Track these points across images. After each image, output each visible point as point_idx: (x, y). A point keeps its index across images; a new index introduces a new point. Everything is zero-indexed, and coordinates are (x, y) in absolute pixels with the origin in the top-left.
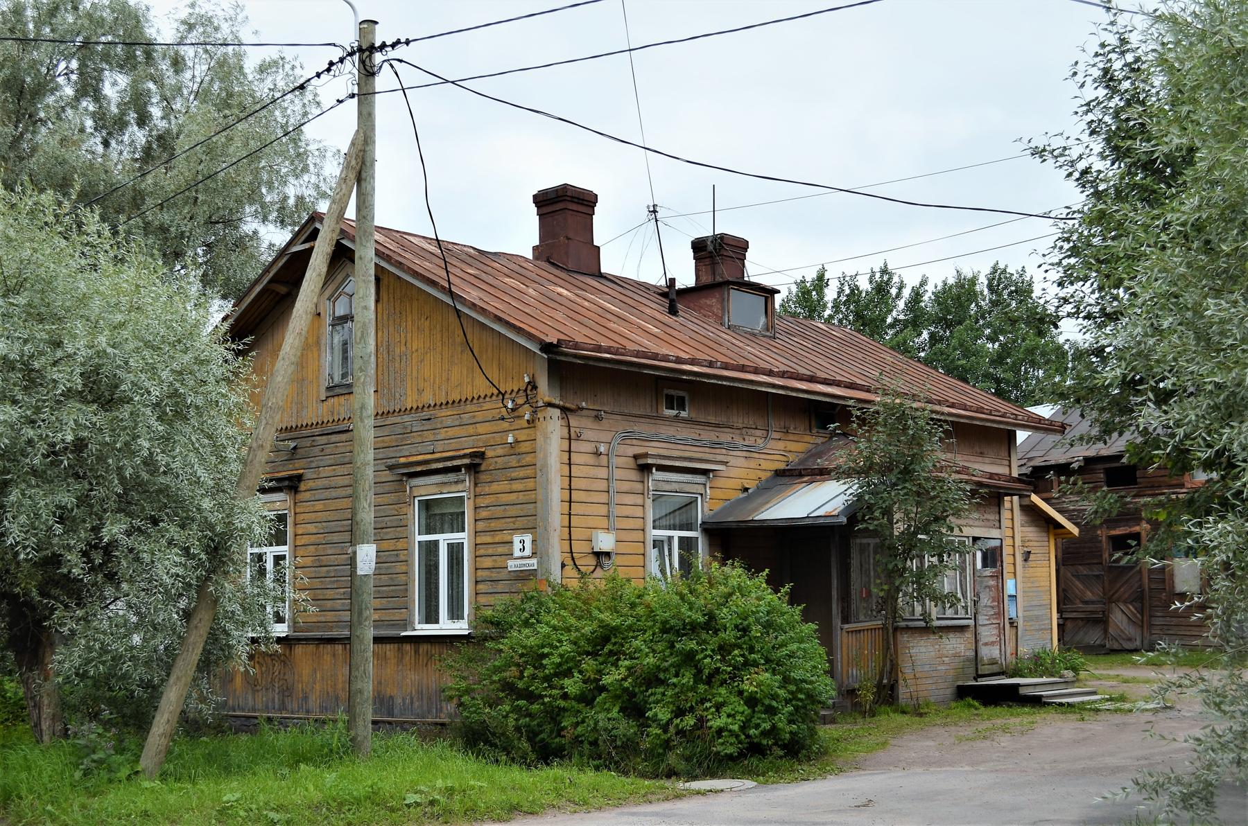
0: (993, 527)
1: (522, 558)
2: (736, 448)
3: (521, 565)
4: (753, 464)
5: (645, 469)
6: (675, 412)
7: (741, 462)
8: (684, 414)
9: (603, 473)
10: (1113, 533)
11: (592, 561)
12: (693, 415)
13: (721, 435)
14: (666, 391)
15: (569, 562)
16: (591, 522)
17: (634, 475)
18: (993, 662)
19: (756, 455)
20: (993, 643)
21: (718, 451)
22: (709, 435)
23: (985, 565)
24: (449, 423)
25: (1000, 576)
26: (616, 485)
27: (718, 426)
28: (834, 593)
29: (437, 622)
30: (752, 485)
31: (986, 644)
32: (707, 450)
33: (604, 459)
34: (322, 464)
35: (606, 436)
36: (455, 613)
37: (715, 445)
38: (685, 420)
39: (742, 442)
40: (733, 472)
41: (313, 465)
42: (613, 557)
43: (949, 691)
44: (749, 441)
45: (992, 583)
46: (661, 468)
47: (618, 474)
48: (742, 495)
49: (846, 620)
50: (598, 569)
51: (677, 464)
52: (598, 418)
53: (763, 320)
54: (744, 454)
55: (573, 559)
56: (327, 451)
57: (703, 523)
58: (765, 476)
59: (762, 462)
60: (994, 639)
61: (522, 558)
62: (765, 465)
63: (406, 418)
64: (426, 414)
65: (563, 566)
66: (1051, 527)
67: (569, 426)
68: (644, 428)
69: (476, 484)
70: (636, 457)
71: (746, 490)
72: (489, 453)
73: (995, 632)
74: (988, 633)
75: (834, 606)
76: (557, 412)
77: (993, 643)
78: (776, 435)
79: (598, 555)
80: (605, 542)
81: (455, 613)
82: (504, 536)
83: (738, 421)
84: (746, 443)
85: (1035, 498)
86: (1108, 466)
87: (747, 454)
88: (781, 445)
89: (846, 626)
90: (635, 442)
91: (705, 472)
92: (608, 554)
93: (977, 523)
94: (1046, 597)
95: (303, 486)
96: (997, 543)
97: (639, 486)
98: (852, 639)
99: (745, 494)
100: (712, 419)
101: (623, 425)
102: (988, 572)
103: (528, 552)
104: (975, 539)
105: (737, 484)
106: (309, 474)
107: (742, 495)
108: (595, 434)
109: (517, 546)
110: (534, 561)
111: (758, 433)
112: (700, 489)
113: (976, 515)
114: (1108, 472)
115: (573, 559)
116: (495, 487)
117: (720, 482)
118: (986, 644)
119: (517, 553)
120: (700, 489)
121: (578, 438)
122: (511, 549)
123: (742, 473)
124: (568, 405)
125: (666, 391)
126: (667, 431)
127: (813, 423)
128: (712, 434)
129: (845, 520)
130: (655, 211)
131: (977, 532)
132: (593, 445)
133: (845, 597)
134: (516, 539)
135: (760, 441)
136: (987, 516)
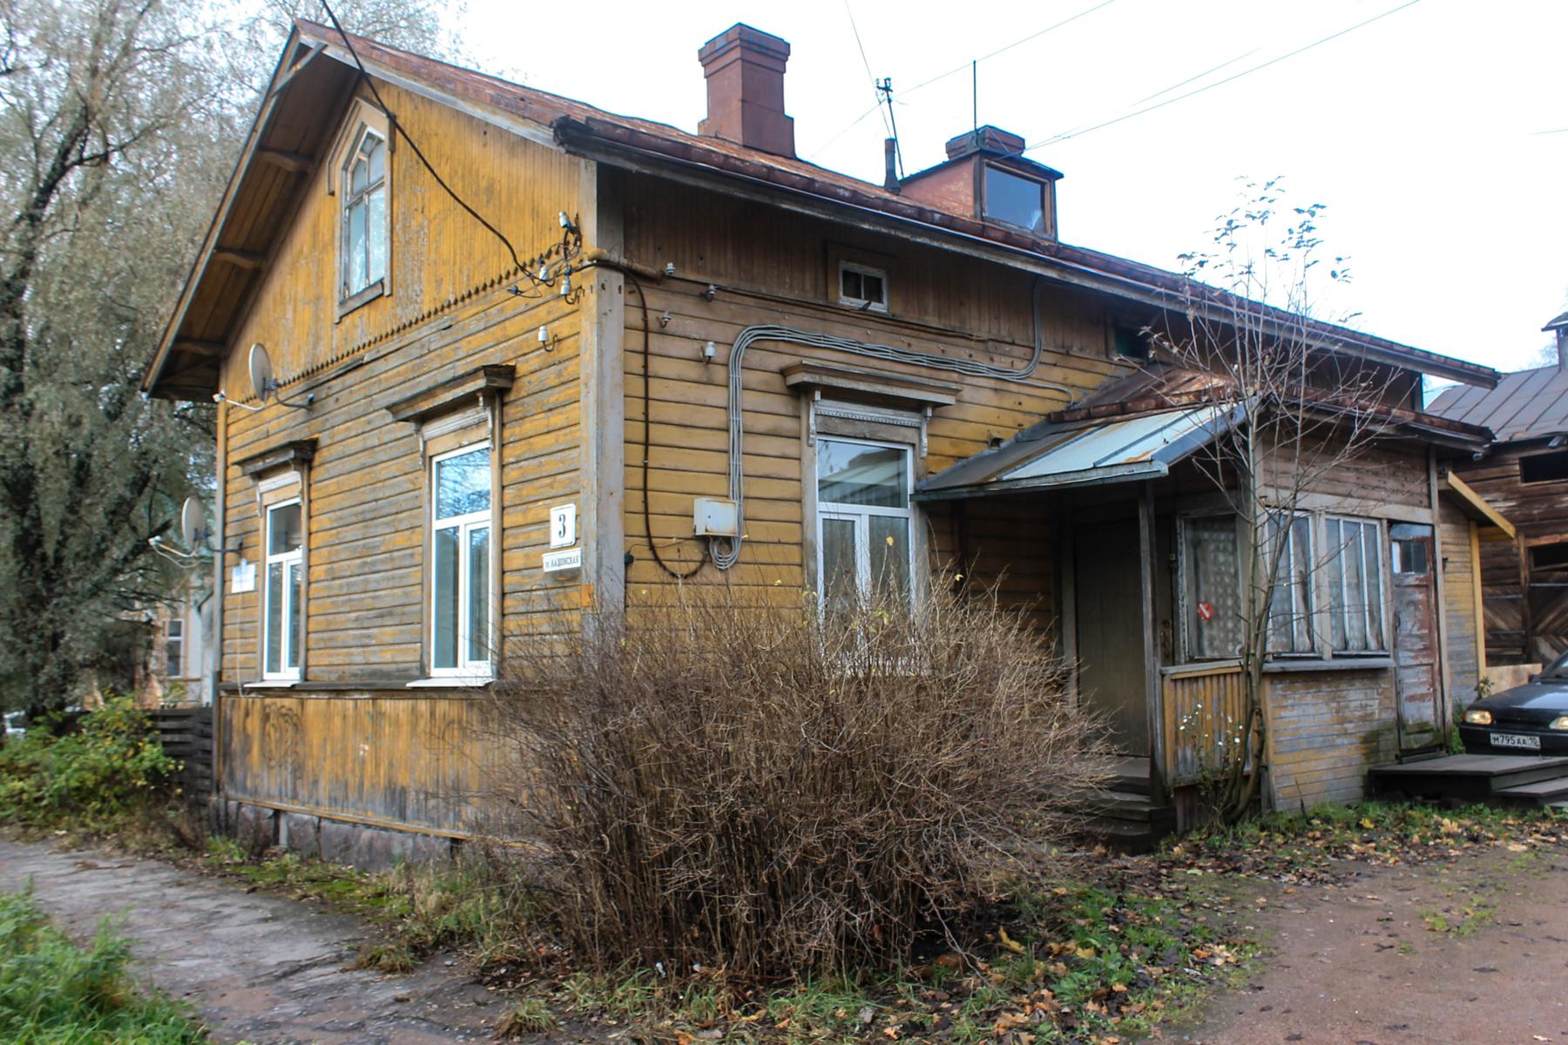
0: (1420, 504)
1: (562, 548)
2: (976, 373)
3: (561, 562)
4: (1008, 402)
5: (800, 393)
6: (861, 303)
7: (988, 397)
8: (875, 307)
9: (717, 396)
10: (1545, 541)
11: (694, 552)
12: (898, 310)
13: (949, 349)
14: (844, 265)
15: (642, 551)
16: (690, 482)
17: (779, 404)
18: (1423, 728)
19: (1013, 388)
20: (1422, 697)
21: (944, 375)
22: (928, 348)
23: (1406, 565)
24: (473, 328)
25: (1430, 585)
26: (740, 420)
27: (942, 333)
28: (1147, 609)
29: (455, 665)
30: (1008, 436)
31: (1412, 698)
32: (924, 372)
33: (719, 374)
34: (336, 421)
35: (726, 333)
36: (478, 653)
37: (937, 364)
38: (878, 316)
39: (987, 363)
40: (971, 413)
41: (328, 425)
42: (737, 547)
43: (1357, 782)
44: (1002, 363)
45: (1419, 596)
46: (831, 393)
47: (750, 400)
48: (987, 451)
49: (1170, 657)
50: (707, 570)
51: (862, 386)
52: (705, 298)
53: (1038, 214)
54: (992, 383)
55: (652, 548)
56: (342, 402)
57: (917, 492)
58: (1028, 422)
59: (1024, 400)
60: (1424, 690)
61: (562, 548)
62: (1029, 404)
63: (425, 331)
64: (445, 320)
65: (629, 560)
66: (1473, 524)
67: (644, 308)
68: (793, 323)
69: (503, 425)
70: (784, 372)
71: (996, 441)
72: (522, 369)
73: (1425, 678)
74: (1415, 681)
75: (1148, 633)
76: (617, 279)
77: (1422, 697)
78: (1049, 358)
79: (705, 540)
80: (716, 517)
81: (478, 653)
82: (534, 512)
83: (982, 327)
84: (995, 365)
85: (1453, 480)
86: (1525, 454)
87: (999, 385)
88: (1057, 374)
89: (1172, 670)
90: (782, 347)
91: (918, 406)
92: (727, 541)
93: (1393, 497)
94: (1469, 625)
95: (318, 459)
96: (1426, 532)
97: (788, 424)
98: (1183, 694)
99: (994, 450)
100: (933, 322)
101: (760, 317)
102: (1412, 578)
103: (569, 538)
104: (1392, 523)
105: (981, 432)
106: (324, 439)
107: (987, 451)
108: (697, 330)
109: (555, 526)
110: (576, 553)
111: (1017, 351)
112: (911, 435)
113: (1391, 484)
114: (1524, 462)
115: (652, 548)
116: (528, 427)
117: (944, 428)
118: (1412, 698)
119: (556, 541)
120: (911, 435)
121: (663, 331)
122: (548, 533)
123: (991, 415)
124: (638, 266)
125: (844, 265)
126: (841, 333)
127: (1112, 343)
128: (933, 346)
129: (1165, 469)
130: (887, 89)
131: (1396, 511)
132: (697, 345)
133: (1168, 618)
134: (555, 513)
135: (1019, 364)
136: (1409, 487)
